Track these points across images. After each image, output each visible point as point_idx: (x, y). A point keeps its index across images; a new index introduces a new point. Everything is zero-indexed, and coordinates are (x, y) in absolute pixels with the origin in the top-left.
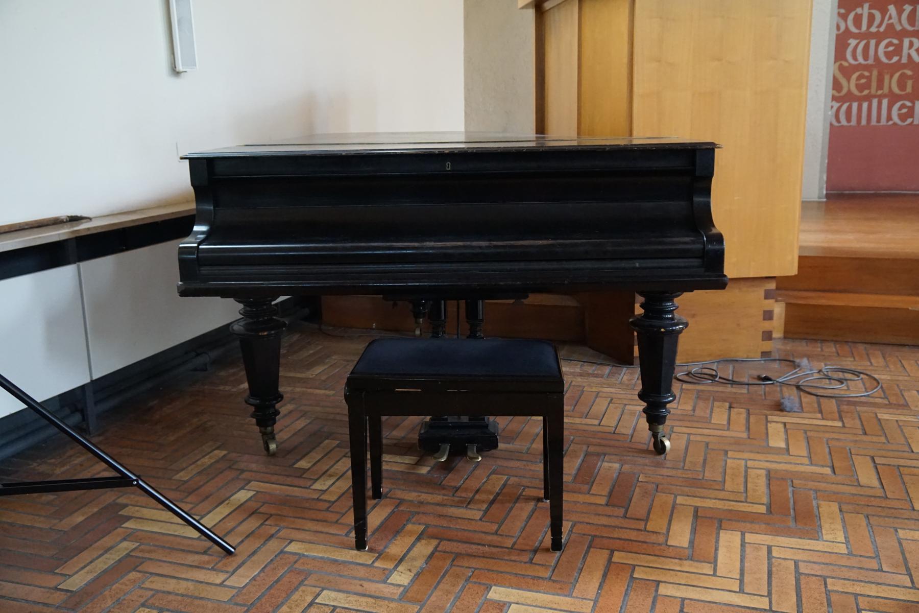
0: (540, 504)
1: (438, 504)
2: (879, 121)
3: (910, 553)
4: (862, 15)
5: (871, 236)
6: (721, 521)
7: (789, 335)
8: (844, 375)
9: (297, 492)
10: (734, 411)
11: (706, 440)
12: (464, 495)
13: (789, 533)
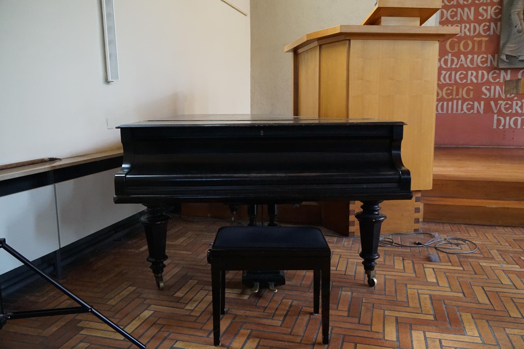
0: (312, 316)
1: (256, 317)
2: (457, 111)
3: (515, 342)
4: (448, 59)
5: (461, 169)
6: (411, 325)
7: (426, 220)
8: (459, 241)
9: (177, 311)
10: (406, 262)
11: (394, 278)
12: (270, 312)
13: (449, 332)
